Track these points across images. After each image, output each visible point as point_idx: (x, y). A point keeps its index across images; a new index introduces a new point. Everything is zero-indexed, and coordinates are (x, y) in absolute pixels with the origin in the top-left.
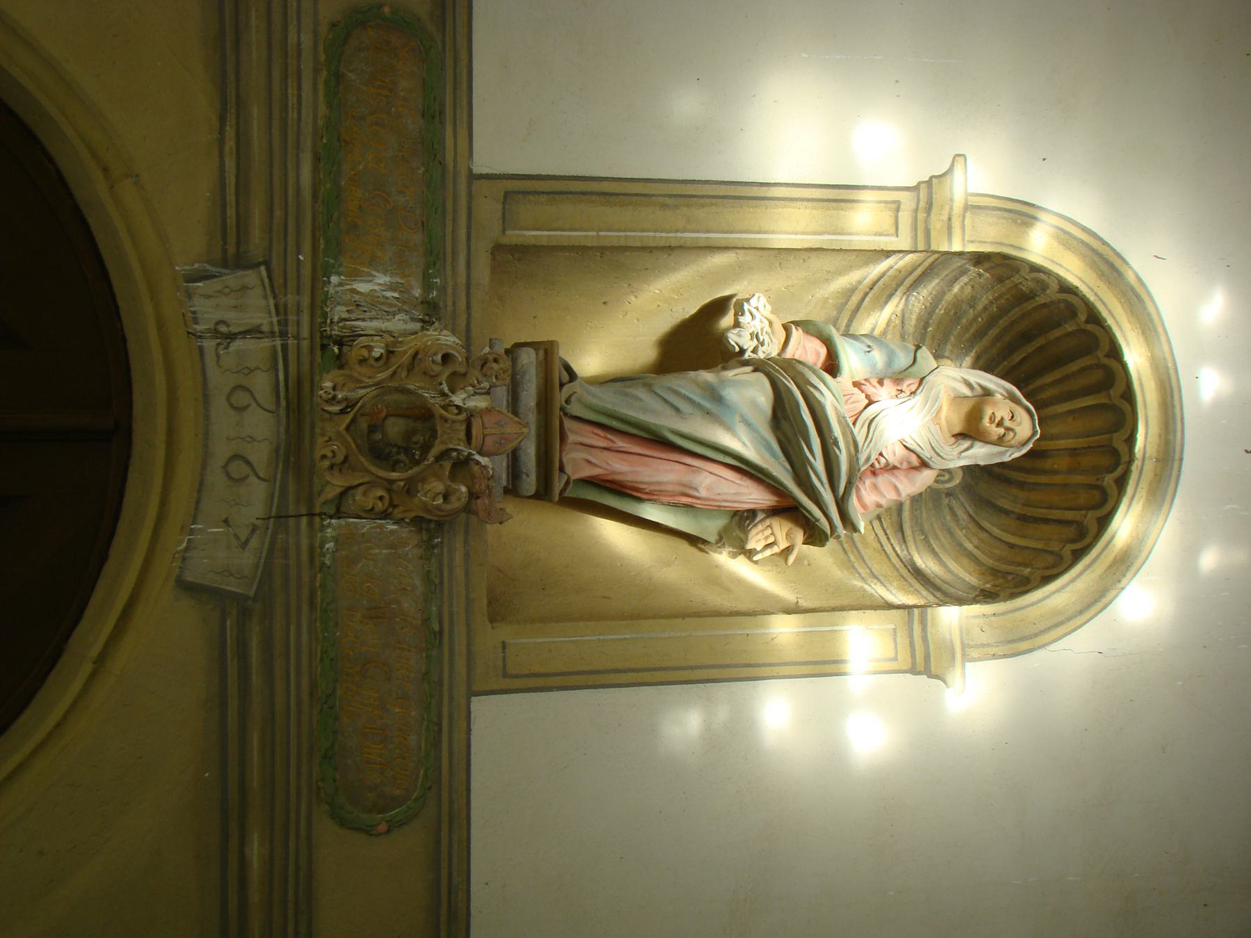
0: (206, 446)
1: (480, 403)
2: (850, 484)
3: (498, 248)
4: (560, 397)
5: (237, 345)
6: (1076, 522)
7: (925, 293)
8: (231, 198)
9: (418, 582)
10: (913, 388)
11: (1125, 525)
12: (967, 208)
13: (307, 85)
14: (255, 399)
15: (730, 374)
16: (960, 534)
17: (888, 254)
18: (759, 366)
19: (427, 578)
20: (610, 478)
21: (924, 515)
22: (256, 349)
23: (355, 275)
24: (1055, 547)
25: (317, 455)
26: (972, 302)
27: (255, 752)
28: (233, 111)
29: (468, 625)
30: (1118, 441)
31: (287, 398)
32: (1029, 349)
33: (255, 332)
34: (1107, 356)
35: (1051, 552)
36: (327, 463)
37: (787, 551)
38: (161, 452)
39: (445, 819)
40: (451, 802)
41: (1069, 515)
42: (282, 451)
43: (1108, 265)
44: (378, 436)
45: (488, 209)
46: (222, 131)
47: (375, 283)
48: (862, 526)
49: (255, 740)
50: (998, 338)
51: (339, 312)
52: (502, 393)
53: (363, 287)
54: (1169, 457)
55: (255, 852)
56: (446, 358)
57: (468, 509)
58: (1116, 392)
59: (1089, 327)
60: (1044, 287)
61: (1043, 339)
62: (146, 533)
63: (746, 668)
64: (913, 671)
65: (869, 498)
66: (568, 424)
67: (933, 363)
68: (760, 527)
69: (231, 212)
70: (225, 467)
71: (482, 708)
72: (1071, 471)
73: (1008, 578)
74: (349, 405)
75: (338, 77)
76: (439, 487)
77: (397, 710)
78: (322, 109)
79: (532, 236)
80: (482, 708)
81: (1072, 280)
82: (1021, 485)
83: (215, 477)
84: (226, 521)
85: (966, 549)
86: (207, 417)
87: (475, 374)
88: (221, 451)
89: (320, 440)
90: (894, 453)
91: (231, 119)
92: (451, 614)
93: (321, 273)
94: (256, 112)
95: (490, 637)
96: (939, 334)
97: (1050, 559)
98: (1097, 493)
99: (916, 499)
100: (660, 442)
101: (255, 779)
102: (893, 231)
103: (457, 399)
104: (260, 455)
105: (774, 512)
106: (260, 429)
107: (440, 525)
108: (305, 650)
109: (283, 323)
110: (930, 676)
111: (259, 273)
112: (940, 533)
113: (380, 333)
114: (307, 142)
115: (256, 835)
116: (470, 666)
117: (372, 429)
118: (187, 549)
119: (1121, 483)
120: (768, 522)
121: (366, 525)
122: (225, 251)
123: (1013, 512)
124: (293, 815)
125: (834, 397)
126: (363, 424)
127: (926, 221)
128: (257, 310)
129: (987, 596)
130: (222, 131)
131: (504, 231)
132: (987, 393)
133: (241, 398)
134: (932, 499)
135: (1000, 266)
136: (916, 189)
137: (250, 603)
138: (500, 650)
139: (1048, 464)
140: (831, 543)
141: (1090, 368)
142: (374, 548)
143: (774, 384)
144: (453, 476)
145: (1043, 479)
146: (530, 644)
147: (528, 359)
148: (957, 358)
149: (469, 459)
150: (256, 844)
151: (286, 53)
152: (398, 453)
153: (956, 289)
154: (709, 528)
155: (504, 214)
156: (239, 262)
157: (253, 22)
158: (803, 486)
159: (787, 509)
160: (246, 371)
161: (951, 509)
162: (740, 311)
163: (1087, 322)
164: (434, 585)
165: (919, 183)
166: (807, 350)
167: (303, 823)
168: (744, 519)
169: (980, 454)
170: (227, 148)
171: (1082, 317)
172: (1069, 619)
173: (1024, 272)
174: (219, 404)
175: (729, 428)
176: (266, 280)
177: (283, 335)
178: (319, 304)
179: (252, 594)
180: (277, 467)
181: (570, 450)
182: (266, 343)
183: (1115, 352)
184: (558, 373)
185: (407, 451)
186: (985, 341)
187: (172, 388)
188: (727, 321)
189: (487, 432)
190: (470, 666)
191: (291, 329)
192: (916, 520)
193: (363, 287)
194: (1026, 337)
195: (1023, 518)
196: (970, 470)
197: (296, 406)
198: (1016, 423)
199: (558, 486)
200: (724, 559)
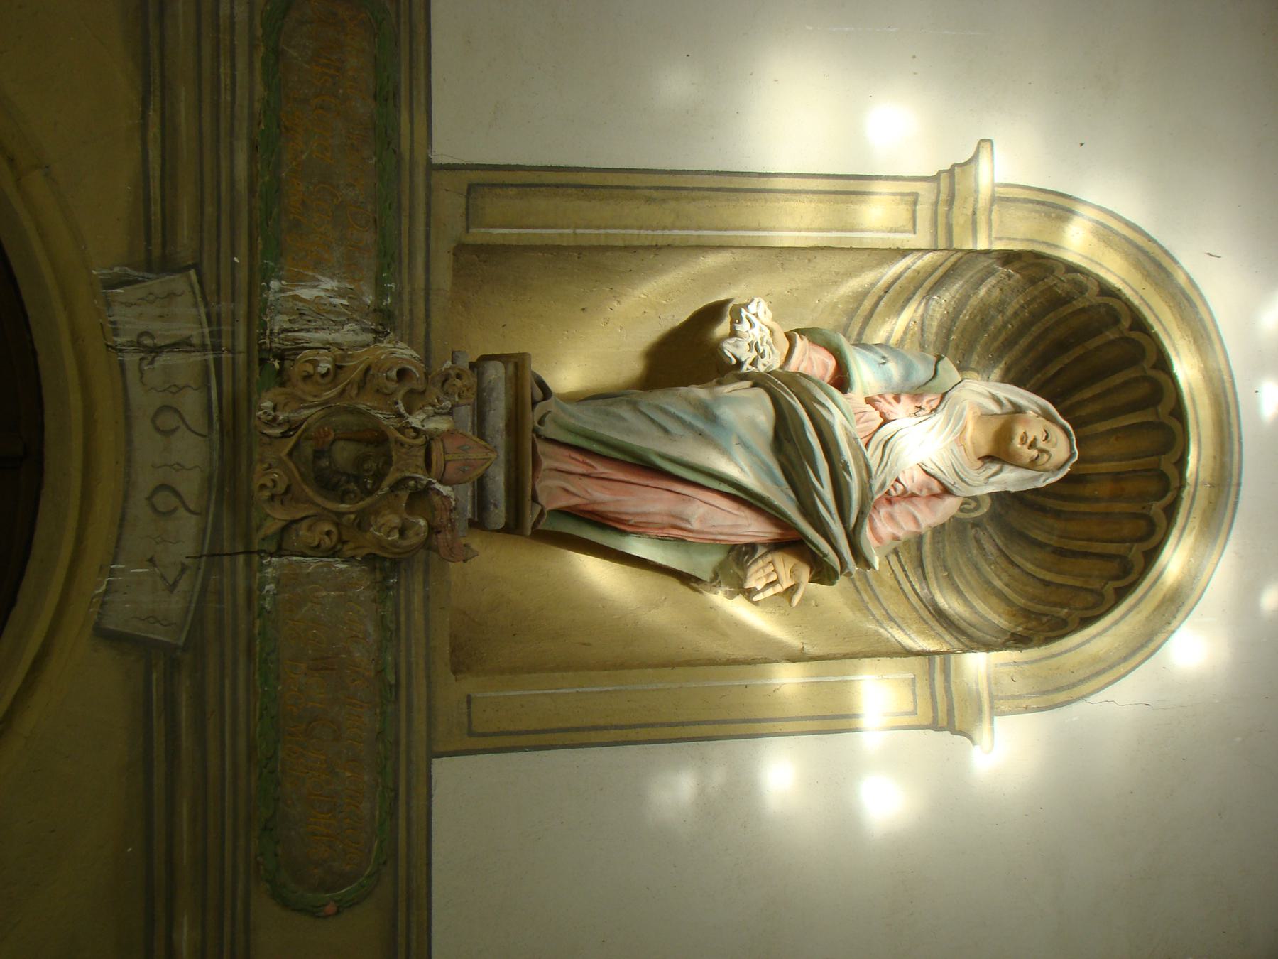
1: (440, 424)
2: (862, 514)
3: (460, 249)
4: (532, 417)
5: (163, 359)
6: (1120, 556)
8: (155, 192)
9: (371, 629)
10: (934, 405)
11: (1175, 560)
12: (995, 200)
15: (726, 390)
16: (988, 570)
17: (904, 253)
18: (759, 381)
20: (589, 508)
21: (948, 548)
22: (184, 365)
23: (298, 279)
24: (1096, 584)
25: (256, 485)
26: (1001, 306)
29: (428, 677)
30: (1167, 464)
32: (1066, 359)
33: (183, 345)
35: (1092, 591)
37: (792, 590)
41: (1112, 548)
42: (215, 480)
43: (1154, 264)
44: (325, 463)
45: (450, 205)
46: (144, 115)
47: (321, 289)
48: (876, 561)
49: (185, 810)
50: (1031, 347)
51: (280, 321)
52: (466, 413)
53: (306, 293)
55: (185, 937)
56: (403, 374)
57: (427, 545)
58: (1164, 409)
60: (1082, 289)
61: (1083, 350)
64: (935, 726)
65: (883, 530)
66: (542, 447)
68: (760, 563)
69: (156, 208)
70: (149, 499)
72: (1114, 498)
74: (293, 427)
76: (395, 520)
77: (348, 774)
78: (260, 90)
79: (499, 234)
81: (1114, 281)
82: (1058, 514)
84: (151, 560)
85: (994, 587)
86: (129, 442)
87: (435, 391)
88: (146, 480)
89: (259, 468)
90: (911, 477)
91: (155, 102)
92: (409, 664)
93: (259, 277)
96: (963, 343)
97: (1090, 599)
98: (1142, 523)
99: (938, 531)
102: (909, 227)
103: (415, 420)
104: (190, 485)
105: (776, 546)
106: (189, 455)
107: (395, 563)
109: (216, 334)
110: (954, 732)
111: (189, 277)
113: (327, 346)
114: (243, 129)
115: (186, 918)
117: (318, 454)
119: (1171, 512)
120: (769, 558)
122: (149, 252)
125: (843, 416)
126: (308, 449)
128: (186, 321)
129: (1018, 641)
130: (144, 115)
131: (468, 229)
132: (1018, 410)
133: (169, 421)
135: (1033, 266)
136: (936, 179)
138: (465, 705)
139: (1087, 490)
140: (842, 581)
141: (1136, 380)
142: (320, 590)
144: (410, 507)
145: (1083, 507)
147: (496, 373)
148: (984, 371)
149: (428, 488)
150: (186, 929)
151: (218, 26)
152: (348, 482)
153: (982, 291)
154: (702, 564)
156: (166, 265)
159: (791, 543)
161: (978, 541)
162: (736, 318)
163: (1131, 329)
165: (940, 173)
166: (813, 362)
168: (742, 554)
169: (1010, 479)
171: (1126, 323)
173: (1060, 273)
176: (197, 287)
177: (216, 348)
178: (257, 312)
179: (181, 643)
181: (550, 476)
182: (197, 357)
183: (1163, 364)
184: (530, 389)
185: (357, 479)
188: (722, 329)
189: (449, 457)
191: (226, 342)
192: (937, 553)
193: (306, 293)
194: (1062, 346)
195: (1060, 552)
196: (1001, 498)
197: (231, 428)
198: (1051, 444)
199: (530, 517)
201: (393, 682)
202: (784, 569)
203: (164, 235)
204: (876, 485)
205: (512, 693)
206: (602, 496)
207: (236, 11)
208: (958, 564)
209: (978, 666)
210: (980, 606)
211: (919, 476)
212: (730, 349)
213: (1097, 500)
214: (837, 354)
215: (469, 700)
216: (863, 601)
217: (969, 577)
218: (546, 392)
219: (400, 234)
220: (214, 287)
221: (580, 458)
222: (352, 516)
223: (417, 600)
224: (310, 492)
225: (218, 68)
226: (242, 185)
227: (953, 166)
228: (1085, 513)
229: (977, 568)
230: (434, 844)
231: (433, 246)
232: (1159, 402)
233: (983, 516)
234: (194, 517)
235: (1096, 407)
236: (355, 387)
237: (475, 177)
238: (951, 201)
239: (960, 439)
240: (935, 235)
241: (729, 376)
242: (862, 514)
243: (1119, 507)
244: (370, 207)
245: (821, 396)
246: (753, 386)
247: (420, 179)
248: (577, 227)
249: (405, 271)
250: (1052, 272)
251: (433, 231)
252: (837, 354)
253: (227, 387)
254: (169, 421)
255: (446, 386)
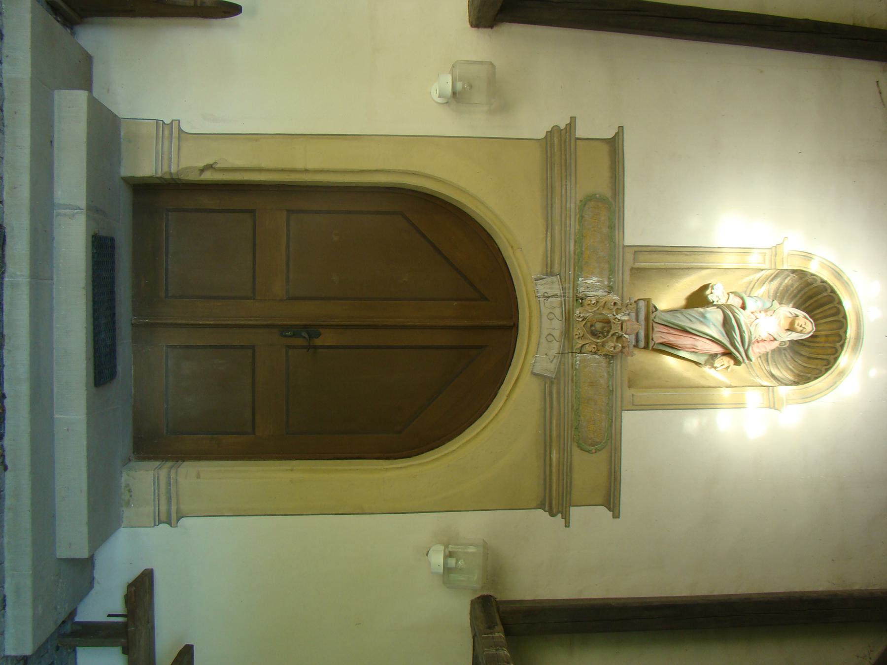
1: (626, 318)
2: (749, 346)
3: (632, 269)
4: (652, 316)
5: (550, 300)
7: (778, 280)
8: (549, 255)
11: (844, 359)
12: (789, 255)
13: (572, 219)
15: (708, 309)
16: (788, 363)
17: (762, 270)
18: (719, 307)
19: (608, 373)
22: (555, 301)
23: (587, 278)
24: (819, 367)
26: (792, 285)
30: (841, 332)
32: (812, 301)
33: (555, 296)
37: (728, 367)
38: (527, 333)
41: (825, 357)
43: (838, 275)
45: (629, 257)
47: (593, 280)
48: (753, 359)
49: (554, 422)
50: (801, 298)
51: (581, 289)
52: (633, 315)
53: (589, 282)
54: (858, 338)
56: (615, 304)
57: (621, 352)
58: (841, 316)
60: (816, 281)
61: (817, 300)
62: (523, 357)
63: (711, 405)
64: (770, 408)
65: (755, 351)
66: (655, 325)
67: (778, 306)
69: (549, 259)
71: (625, 414)
72: (826, 342)
73: (804, 377)
74: (585, 318)
75: (582, 217)
76: (613, 345)
78: (577, 227)
79: (643, 265)
80: (625, 414)
81: (825, 279)
82: (809, 347)
83: (543, 340)
86: (541, 322)
87: (624, 309)
88: (545, 332)
89: (575, 330)
90: (764, 336)
91: (549, 230)
93: (576, 277)
94: (557, 228)
95: (628, 393)
96: (781, 296)
99: (773, 351)
100: (685, 331)
103: (618, 317)
104: (557, 334)
105: (724, 354)
106: (557, 326)
107: (613, 356)
109: (564, 293)
113: (594, 296)
114: (572, 237)
116: (622, 402)
117: (592, 326)
119: (842, 346)
121: (589, 356)
125: (743, 316)
126: (589, 325)
128: (556, 289)
129: (796, 383)
132: (797, 316)
133: (552, 316)
134: (778, 351)
135: (800, 274)
139: (818, 340)
140: (743, 365)
142: (592, 364)
143: (724, 312)
144: (617, 341)
146: (641, 395)
147: (642, 304)
148: (787, 304)
149: (622, 336)
153: (786, 281)
154: (702, 359)
156: (551, 274)
158: (732, 349)
159: (728, 354)
162: (712, 289)
164: (611, 376)
166: (735, 302)
168: (714, 356)
169: (795, 336)
171: (829, 291)
173: (809, 276)
174: (544, 319)
175: (708, 327)
177: (564, 296)
178: (575, 287)
181: (656, 334)
182: (559, 299)
183: (840, 303)
184: (652, 309)
185: (602, 333)
186: (796, 299)
187: (530, 313)
188: (708, 292)
190: (622, 402)
191: (567, 295)
192: (772, 357)
193: (589, 282)
194: (811, 297)
195: (810, 358)
196: (792, 341)
197: (568, 318)
198: (806, 326)
199: (651, 345)
200: (707, 369)
202: (726, 360)
204: (753, 337)
206: (672, 339)
209: (784, 391)
210: (785, 374)
211: (767, 335)
212: (711, 298)
214: (742, 298)
218: (656, 309)
223: (619, 367)
224: (589, 336)
226: (572, 252)
229: (784, 362)
235: (820, 315)
237: (636, 249)
238: (776, 255)
239: (779, 324)
242: (749, 346)
245: (736, 311)
247: (621, 250)
252: (742, 298)
254: (552, 316)
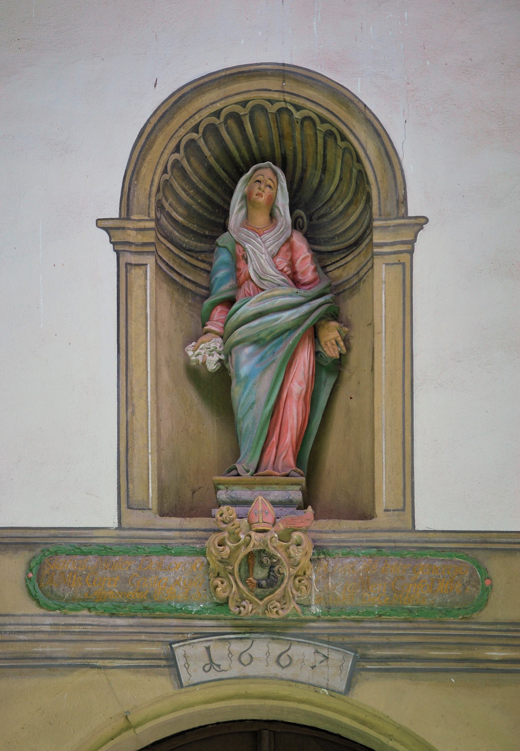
0: (271, 678)
6: (325, 136)
9: (348, 560)
10: (241, 249)
13: (73, 621)
14: (285, 652)
19: (346, 555)
20: (294, 445)
21: (324, 236)
24: (340, 152)
25: (276, 616)
27: (442, 653)
28: (89, 661)
29: (374, 531)
31: (244, 633)
34: (218, 118)
35: (343, 154)
36: (281, 612)
39: (484, 546)
40: (475, 542)
41: (320, 141)
42: (274, 636)
44: (264, 583)
46: (99, 667)
55: (497, 654)
59: (201, 130)
68: (326, 349)
70: (283, 668)
77: (421, 573)
83: (288, 673)
84: (313, 667)
85: (343, 210)
86: (255, 677)
88: (274, 670)
92: (367, 541)
94: (90, 648)
97: (347, 155)
98: (306, 123)
101: (456, 653)
102: (143, 267)
104: (276, 648)
106: (262, 648)
108: (384, 625)
110: (415, 240)
111: (176, 648)
112: (334, 227)
115: (488, 653)
117: (259, 586)
118: (327, 689)
120: (323, 343)
122: (165, 666)
123: (321, 176)
124: (477, 633)
127: (137, 245)
128: (198, 649)
130: (99, 667)
131: (150, 509)
133: (245, 658)
136: (118, 252)
137: (357, 655)
138: (389, 513)
141: (227, 129)
145: (299, 157)
150: (494, 654)
151: (55, 632)
152: (273, 571)
155: (140, 509)
156: (171, 660)
157: (40, 650)
160: (230, 655)
161: (319, 218)
163: (197, 132)
165: (115, 250)
167: (482, 627)
170: (109, 664)
172: (383, 144)
174: (249, 671)
176: (181, 644)
179: (353, 654)
180: (282, 639)
189: (261, 521)
197: (249, 629)
201: (375, 550)
203: (156, 659)
205: (384, 488)
207: (48, 623)
208: (331, 230)
213: (295, 148)
214: (214, 305)
215: (386, 510)
216: (349, 288)
217: (338, 224)
219: (153, 544)
220: (180, 636)
221: (268, 449)
222: (291, 569)
223: (335, 537)
225: (76, 632)
226: (131, 621)
227: (111, 242)
228: (303, 155)
229: (334, 219)
230: (33, 526)
231: (158, 527)
232: (238, 114)
233: (305, 214)
234: (292, 647)
236: (227, 567)
237: (124, 506)
240: (148, 253)
241: (227, 366)
243: (298, 135)
244: (140, 559)
246: (231, 354)
248: (148, 452)
249: (171, 542)
250: (167, 180)
251: (151, 527)
253: (229, 630)
254: (245, 658)
255: (226, 522)
